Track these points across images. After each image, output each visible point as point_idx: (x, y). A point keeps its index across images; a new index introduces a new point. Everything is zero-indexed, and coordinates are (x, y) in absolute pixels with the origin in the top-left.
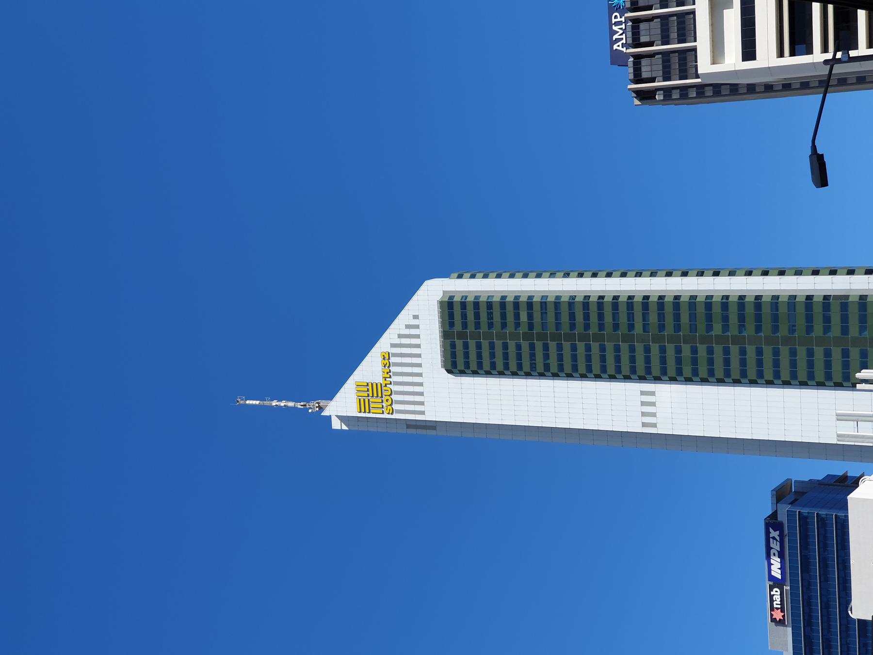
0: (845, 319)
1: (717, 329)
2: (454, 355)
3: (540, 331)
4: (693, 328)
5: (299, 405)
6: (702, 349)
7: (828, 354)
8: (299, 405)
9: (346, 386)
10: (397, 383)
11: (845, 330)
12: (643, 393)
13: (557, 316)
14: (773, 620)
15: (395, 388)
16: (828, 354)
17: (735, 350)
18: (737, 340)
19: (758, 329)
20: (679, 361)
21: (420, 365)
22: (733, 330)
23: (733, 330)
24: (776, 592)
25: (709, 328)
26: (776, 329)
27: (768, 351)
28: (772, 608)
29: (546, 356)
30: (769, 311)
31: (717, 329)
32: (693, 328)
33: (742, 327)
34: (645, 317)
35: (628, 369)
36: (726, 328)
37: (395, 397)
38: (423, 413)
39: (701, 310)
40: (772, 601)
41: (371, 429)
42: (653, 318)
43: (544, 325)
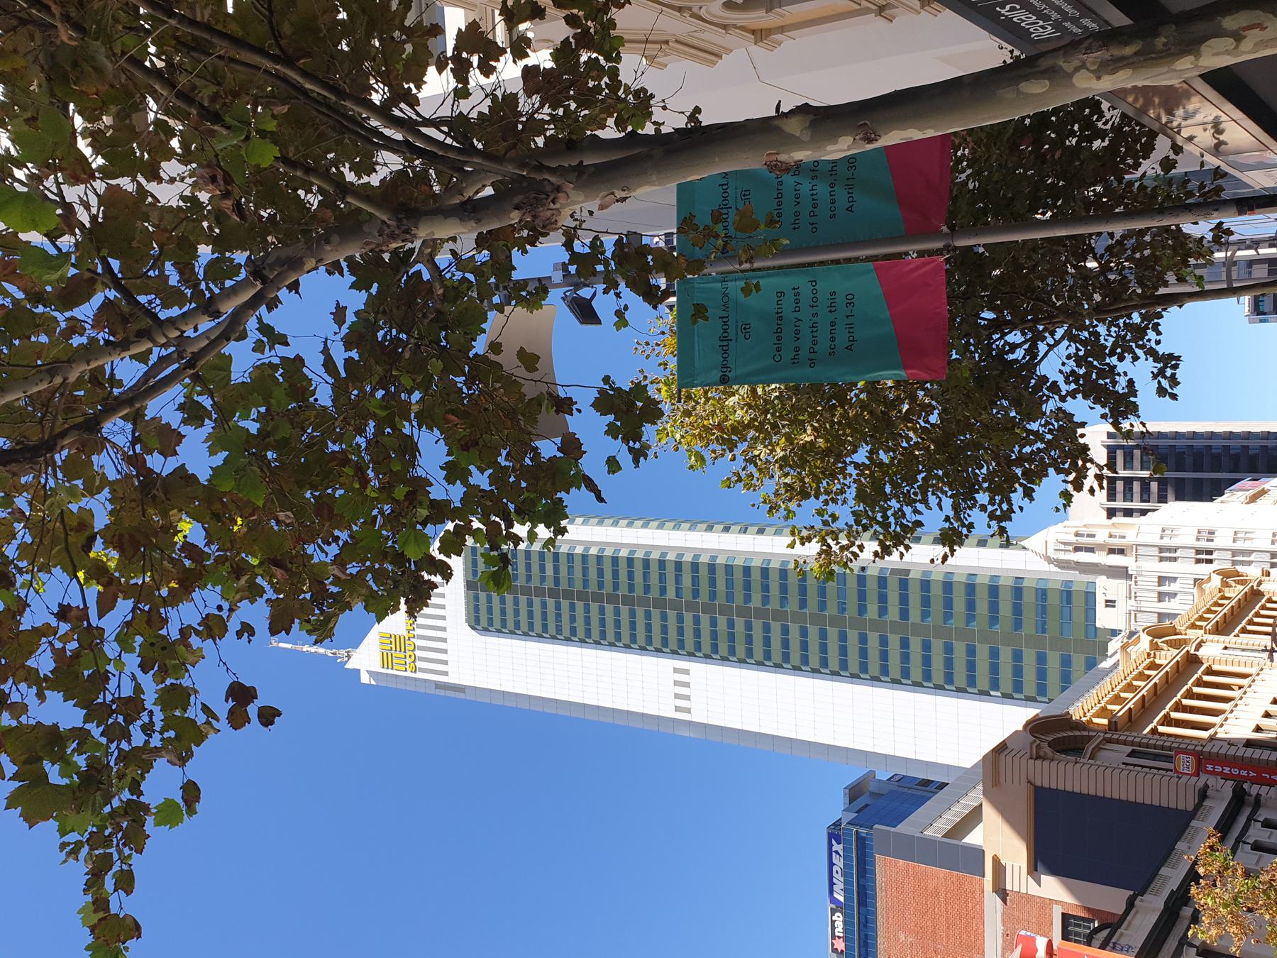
0: (904, 600)
1: (756, 601)
2: (477, 609)
3: (524, 583)
4: (730, 597)
5: (329, 653)
6: (740, 624)
7: (884, 641)
8: (329, 653)
9: (369, 636)
10: (420, 637)
11: (904, 614)
12: (676, 670)
13: (585, 571)
14: (834, 950)
15: (419, 643)
16: (884, 641)
17: (776, 627)
18: (779, 616)
19: (803, 604)
20: (714, 635)
21: (443, 618)
22: (774, 604)
23: (774, 604)
24: (839, 918)
25: (748, 598)
26: (822, 606)
27: (813, 631)
28: (833, 937)
29: (573, 619)
30: (1033, 600)
31: (756, 601)
32: (730, 597)
33: (784, 601)
34: (678, 579)
35: (899, 671)
36: (766, 600)
37: (418, 653)
38: (446, 674)
39: (738, 576)
40: (833, 928)
41: (399, 687)
42: (687, 581)
43: (571, 581)
